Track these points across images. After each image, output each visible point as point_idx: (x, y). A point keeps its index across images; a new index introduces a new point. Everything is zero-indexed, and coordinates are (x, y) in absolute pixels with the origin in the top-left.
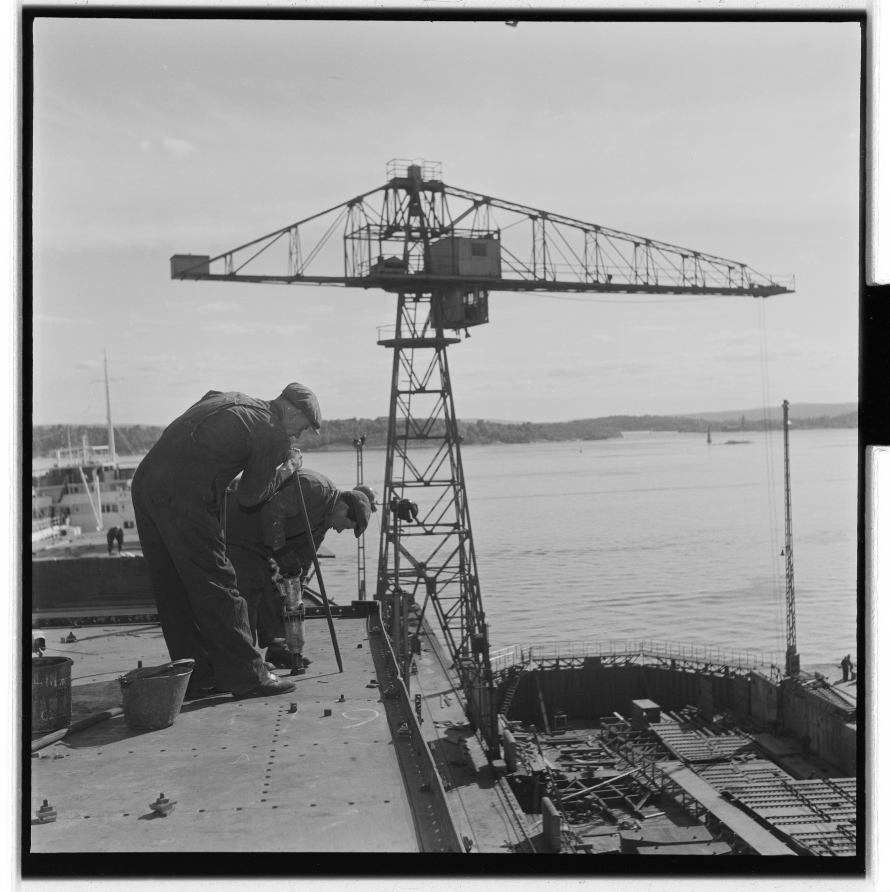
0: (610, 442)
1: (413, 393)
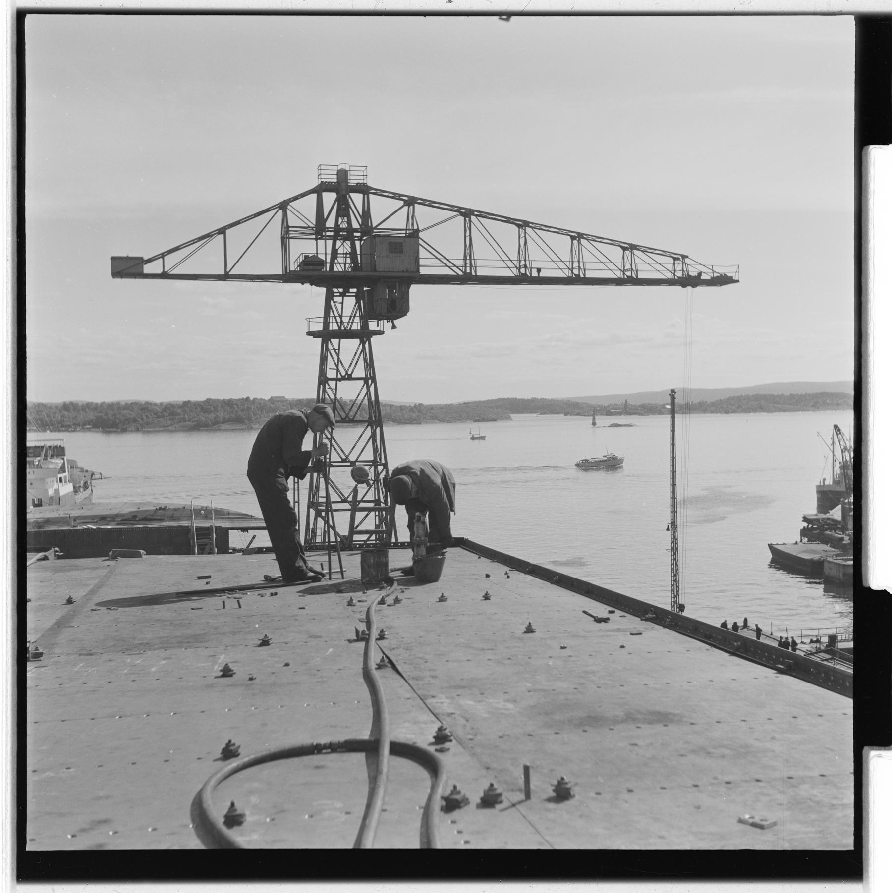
1: (340, 380)
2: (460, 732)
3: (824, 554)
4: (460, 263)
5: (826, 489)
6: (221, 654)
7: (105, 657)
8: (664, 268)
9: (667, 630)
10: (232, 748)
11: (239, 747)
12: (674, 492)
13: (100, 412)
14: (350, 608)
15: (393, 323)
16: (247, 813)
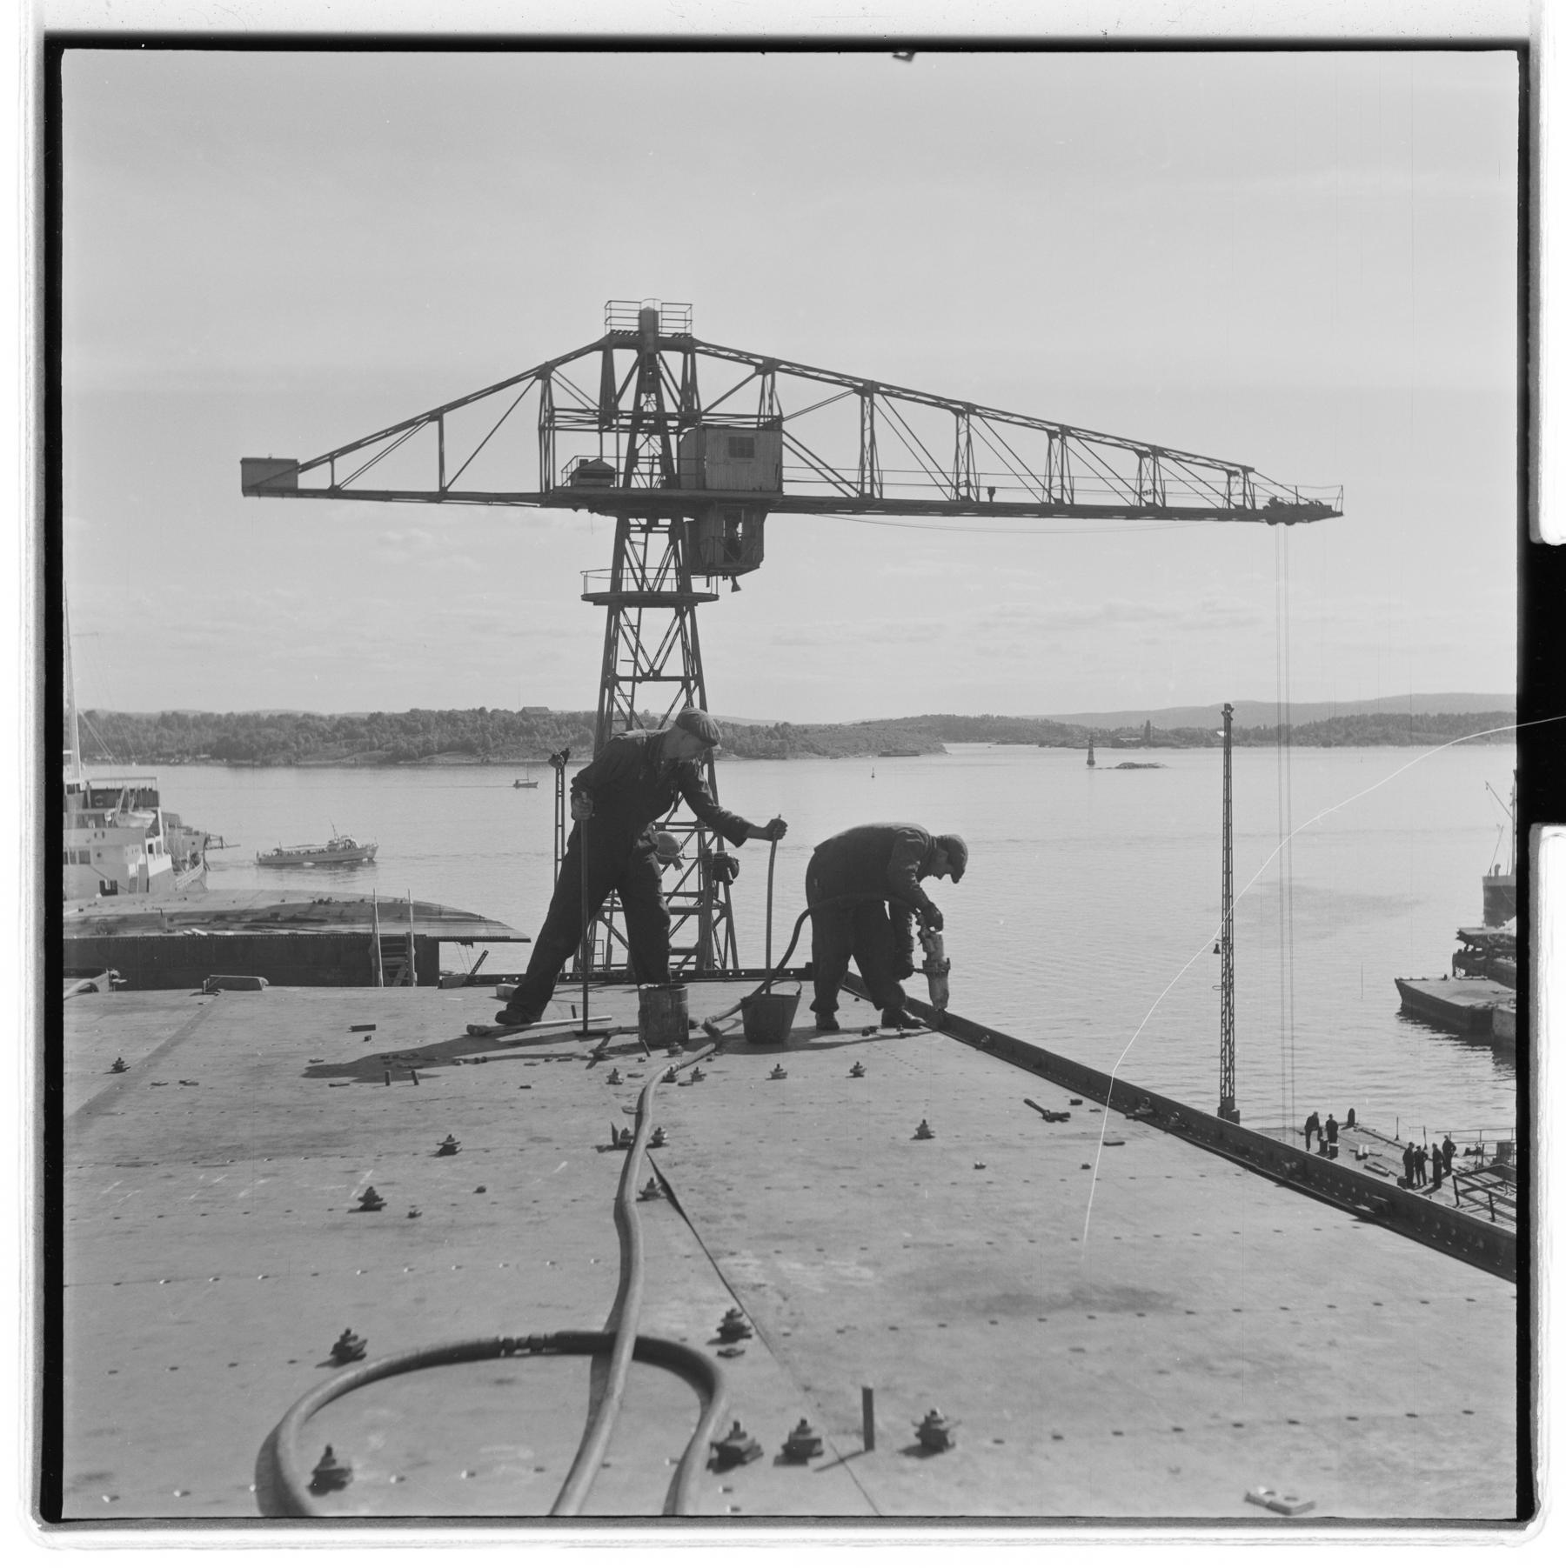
0: (924, 760)
1: (640, 680)
2: (768, 1320)
3: (1494, 999)
4: (853, 476)
5: (1500, 883)
6: (368, 1167)
7: (163, 1170)
8: (1209, 490)
9: (1171, 1138)
10: (351, 1344)
11: (365, 1342)
12: (1227, 884)
13: (226, 730)
14: (612, 1087)
15: (734, 581)
16: (357, 1465)
